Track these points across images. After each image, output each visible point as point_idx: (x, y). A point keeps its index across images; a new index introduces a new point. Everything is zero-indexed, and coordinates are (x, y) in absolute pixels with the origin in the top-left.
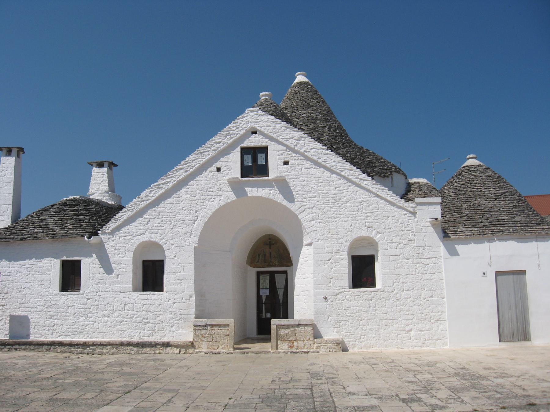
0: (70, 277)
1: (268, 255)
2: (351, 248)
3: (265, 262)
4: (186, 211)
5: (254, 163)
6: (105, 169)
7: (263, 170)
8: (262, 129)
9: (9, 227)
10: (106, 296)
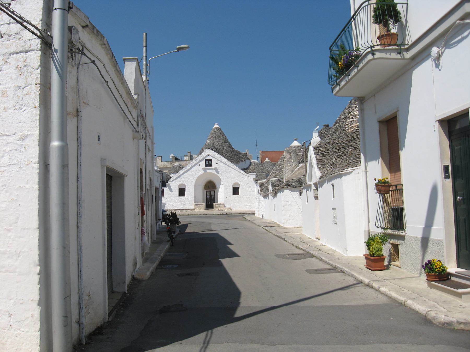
5: (209, 163)
7: (211, 165)
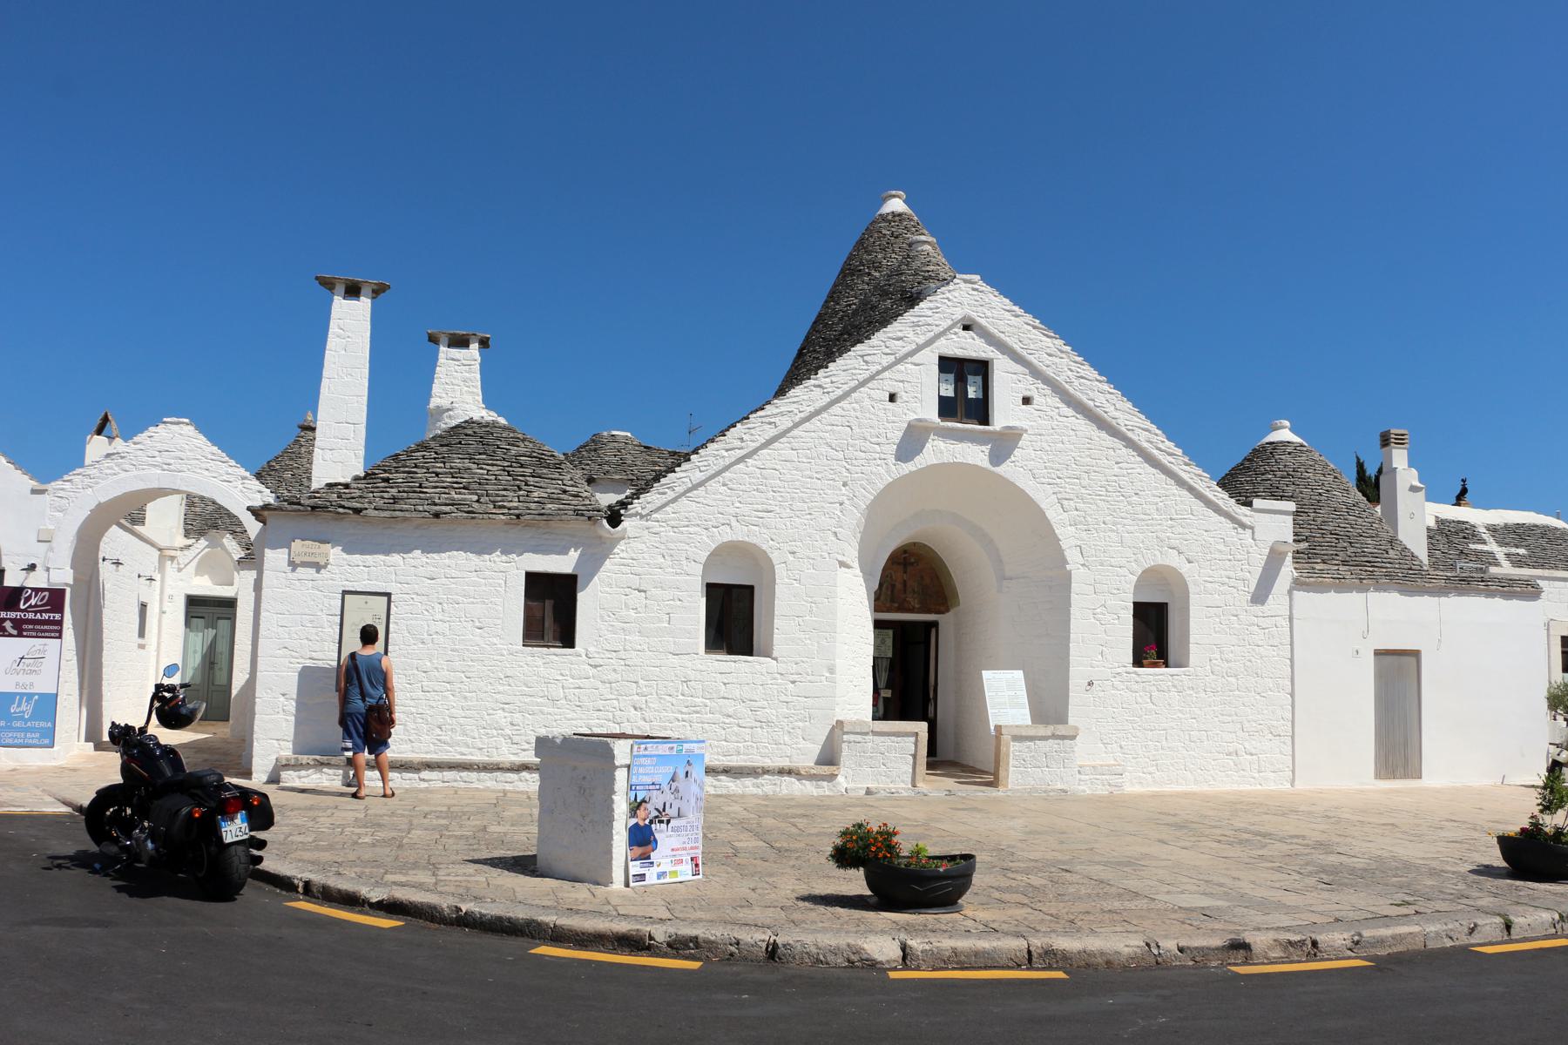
0: (552, 610)
1: (899, 586)
3: (893, 601)
4: (810, 480)
5: (966, 392)
7: (980, 411)
8: (983, 322)
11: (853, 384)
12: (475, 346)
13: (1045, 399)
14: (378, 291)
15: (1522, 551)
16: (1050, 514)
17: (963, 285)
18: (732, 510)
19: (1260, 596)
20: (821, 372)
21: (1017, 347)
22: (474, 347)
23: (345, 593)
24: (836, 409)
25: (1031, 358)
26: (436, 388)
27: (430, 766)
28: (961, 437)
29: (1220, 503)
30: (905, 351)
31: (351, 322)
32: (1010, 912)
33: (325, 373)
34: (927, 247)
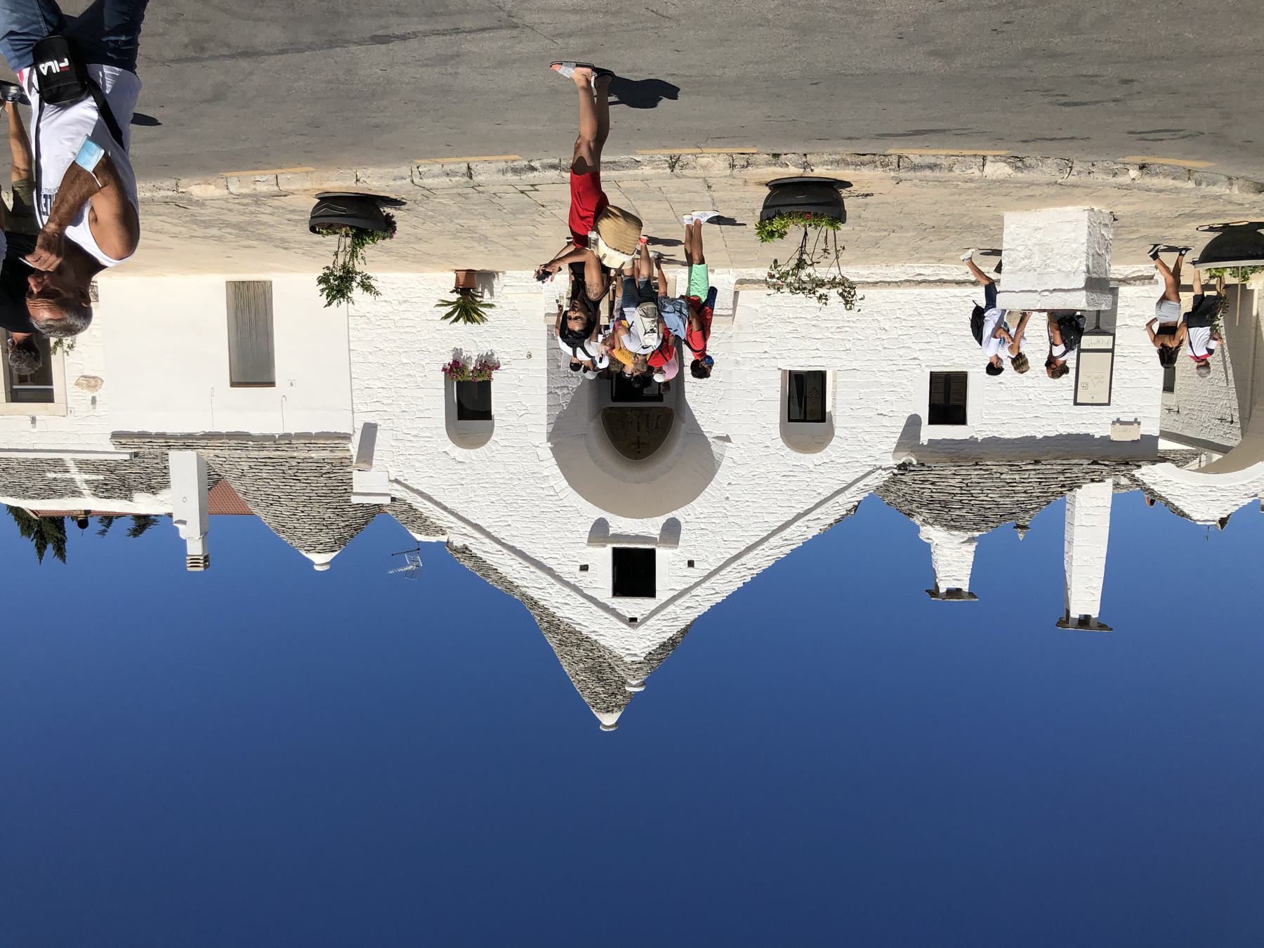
2: (830, 434)
5: (634, 572)
6: (1075, 614)
9: (1074, 486)
10: (884, 363)
11: (724, 572)
12: (942, 590)
13: (569, 571)
14: (1065, 620)
15: (51, 475)
16: (565, 483)
17: (638, 652)
18: (814, 475)
19: (370, 431)
20: (748, 579)
21: (594, 608)
22: (942, 590)
23: (1108, 404)
24: (735, 552)
25: (582, 600)
26: (971, 558)
27: (898, 284)
28: (637, 538)
29: (420, 499)
30: (683, 599)
31: (1085, 599)
32: (524, 177)
33: (1104, 561)
34: (634, 683)
